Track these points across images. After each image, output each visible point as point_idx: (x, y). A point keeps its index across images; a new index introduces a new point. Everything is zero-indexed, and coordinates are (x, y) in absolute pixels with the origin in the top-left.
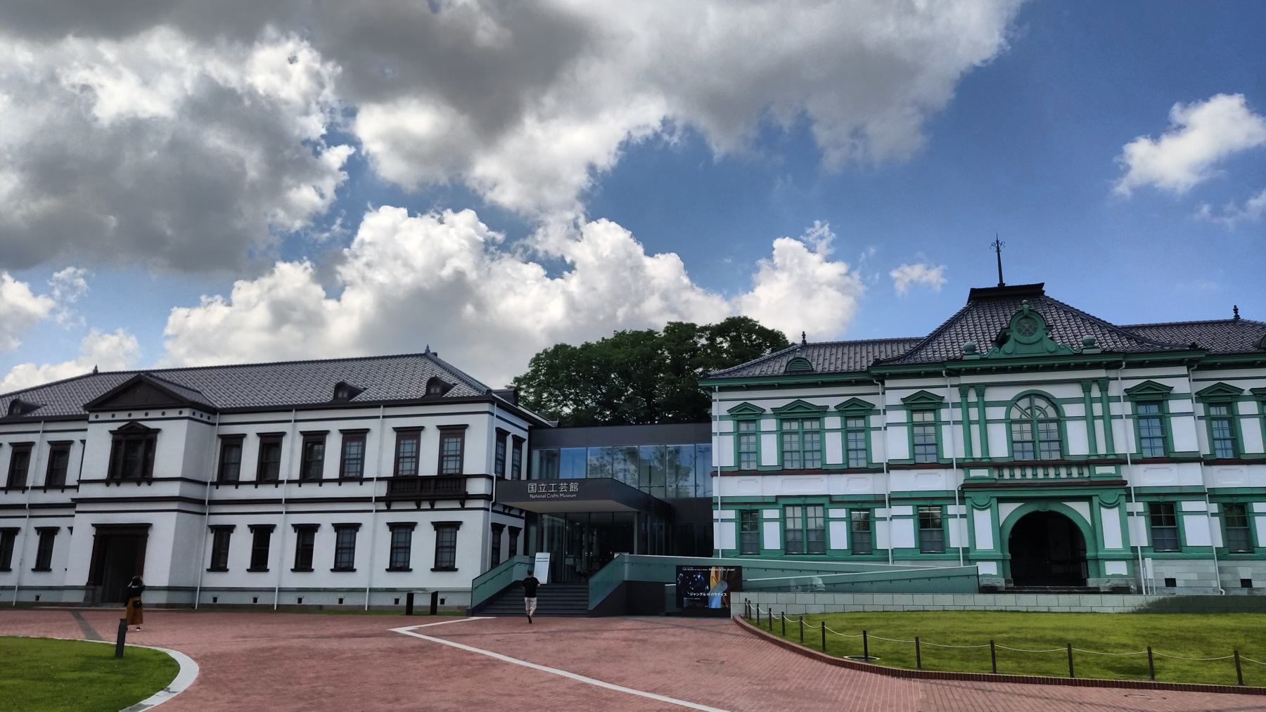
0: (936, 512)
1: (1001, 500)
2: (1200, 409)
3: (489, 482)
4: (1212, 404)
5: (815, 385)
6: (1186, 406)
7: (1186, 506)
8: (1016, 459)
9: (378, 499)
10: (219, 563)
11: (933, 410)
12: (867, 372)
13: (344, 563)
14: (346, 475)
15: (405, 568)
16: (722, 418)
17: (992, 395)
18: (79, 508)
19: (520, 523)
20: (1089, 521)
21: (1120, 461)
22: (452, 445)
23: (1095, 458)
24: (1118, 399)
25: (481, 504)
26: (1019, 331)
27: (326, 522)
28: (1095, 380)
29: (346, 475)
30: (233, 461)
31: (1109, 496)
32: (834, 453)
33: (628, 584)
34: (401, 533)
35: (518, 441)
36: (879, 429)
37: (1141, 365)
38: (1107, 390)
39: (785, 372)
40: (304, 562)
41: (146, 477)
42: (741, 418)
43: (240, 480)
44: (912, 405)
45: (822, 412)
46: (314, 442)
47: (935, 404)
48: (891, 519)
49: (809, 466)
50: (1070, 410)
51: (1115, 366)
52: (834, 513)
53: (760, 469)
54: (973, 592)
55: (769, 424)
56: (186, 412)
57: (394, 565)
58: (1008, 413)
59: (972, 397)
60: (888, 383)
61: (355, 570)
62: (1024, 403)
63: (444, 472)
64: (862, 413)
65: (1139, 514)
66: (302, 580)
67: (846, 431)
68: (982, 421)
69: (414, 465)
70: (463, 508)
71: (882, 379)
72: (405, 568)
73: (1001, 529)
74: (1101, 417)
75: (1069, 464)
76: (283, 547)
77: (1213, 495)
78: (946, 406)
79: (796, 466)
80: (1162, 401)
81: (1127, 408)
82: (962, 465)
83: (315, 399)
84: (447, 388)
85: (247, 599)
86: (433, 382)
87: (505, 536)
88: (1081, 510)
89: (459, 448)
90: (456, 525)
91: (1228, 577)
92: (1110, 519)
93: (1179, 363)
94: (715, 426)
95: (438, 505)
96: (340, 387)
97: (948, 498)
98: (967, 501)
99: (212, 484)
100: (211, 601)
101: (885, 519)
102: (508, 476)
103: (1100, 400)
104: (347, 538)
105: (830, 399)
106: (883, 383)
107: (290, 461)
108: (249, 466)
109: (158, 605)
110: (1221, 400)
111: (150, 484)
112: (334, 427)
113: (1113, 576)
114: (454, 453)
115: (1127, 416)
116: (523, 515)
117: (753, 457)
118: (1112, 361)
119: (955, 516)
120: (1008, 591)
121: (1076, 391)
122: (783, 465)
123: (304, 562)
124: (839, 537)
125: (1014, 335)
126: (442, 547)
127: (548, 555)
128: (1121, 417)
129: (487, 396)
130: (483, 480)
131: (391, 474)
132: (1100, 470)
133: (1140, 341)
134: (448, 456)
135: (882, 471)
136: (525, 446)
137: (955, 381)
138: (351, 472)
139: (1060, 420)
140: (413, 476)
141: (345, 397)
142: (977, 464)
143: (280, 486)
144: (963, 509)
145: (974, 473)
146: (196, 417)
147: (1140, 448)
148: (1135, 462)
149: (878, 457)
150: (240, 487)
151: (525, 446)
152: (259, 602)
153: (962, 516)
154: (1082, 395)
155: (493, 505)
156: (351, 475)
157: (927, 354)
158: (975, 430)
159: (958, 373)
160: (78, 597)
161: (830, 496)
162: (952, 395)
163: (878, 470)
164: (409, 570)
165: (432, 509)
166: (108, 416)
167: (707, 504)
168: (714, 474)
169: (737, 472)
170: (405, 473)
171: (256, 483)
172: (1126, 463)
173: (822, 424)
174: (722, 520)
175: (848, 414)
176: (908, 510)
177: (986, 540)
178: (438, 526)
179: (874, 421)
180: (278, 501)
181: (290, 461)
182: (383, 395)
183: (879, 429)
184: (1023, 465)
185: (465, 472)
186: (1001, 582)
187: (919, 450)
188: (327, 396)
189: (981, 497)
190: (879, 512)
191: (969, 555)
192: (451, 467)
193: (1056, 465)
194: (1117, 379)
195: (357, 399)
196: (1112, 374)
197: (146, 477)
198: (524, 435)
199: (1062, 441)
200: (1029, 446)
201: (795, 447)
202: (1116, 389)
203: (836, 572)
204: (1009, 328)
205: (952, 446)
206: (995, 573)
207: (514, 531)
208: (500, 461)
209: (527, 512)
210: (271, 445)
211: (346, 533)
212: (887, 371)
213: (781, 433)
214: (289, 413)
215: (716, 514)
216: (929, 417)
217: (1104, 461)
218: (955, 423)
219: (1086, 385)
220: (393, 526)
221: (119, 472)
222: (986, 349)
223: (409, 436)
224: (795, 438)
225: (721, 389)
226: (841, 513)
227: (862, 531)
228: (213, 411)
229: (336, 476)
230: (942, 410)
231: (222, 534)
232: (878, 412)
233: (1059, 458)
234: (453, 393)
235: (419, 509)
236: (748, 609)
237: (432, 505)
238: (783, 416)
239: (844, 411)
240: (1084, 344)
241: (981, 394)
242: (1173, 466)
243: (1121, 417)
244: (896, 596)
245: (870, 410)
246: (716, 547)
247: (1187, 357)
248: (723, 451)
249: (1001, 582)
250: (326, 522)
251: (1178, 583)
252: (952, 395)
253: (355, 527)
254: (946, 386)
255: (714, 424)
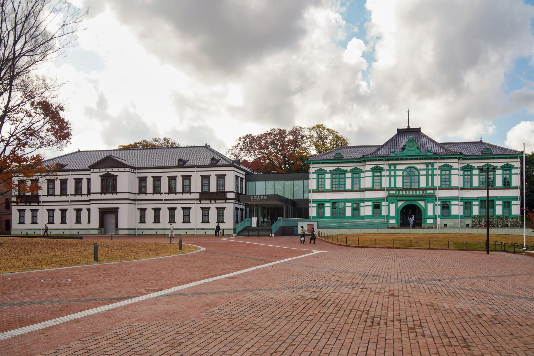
0: (448, 203)
1: (398, 201)
2: (461, 172)
3: (234, 194)
4: (504, 170)
5: (343, 163)
6: (456, 172)
7: (453, 203)
8: (404, 188)
9: (197, 199)
10: (142, 220)
11: (449, 170)
12: (360, 159)
13: (186, 220)
14: (185, 191)
15: (23, 223)
16: (313, 173)
17: (399, 167)
18: (92, 202)
19: (243, 207)
20: (424, 207)
21: (435, 189)
22: (221, 182)
23: (433, 188)
24: (436, 169)
25: (232, 201)
26: (409, 146)
27: (57, 208)
28: (430, 163)
29: (185, 191)
30: (79, 187)
31: (430, 199)
32: (349, 186)
33: (282, 227)
34: (205, 211)
35: (242, 179)
36: (363, 177)
37: (444, 158)
38: (433, 166)
39: (334, 158)
40: (172, 220)
41: (114, 191)
42: (354, 172)
43: (55, 194)
44: (374, 170)
45: (346, 171)
46: (172, 179)
47: (381, 170)
48: (365, 206)
49: (341, 189)
50: (422, 173)
51: (437, 159)
52: (348, 204)
53: (360, 190)
54: (386, 228)
55: (328, 176)
56: (127, 169)
57: (184, 221)
58: (403, 173)
59: (392, 168)
60: (367, 163)
61: (38, 223)
62: (408, 170)
63: (219, 190)
64: (358, 172)
65: (439, 205)
66: (78, 226)
67: (353, 178)
68: (433, 175)
69: (189, 188)
70: (226, 203)
71: (365, 161)
72: (23, 223)
73: (398, 210)
74: (429, 175)
75: (419, 189)
76: (164, 215)
77: (462, 199)
78: (384, 170)
79: (337, 189)
80: (510, 170)
81: (439, 172)
82: (388, 190)
83: (170, 164)
84: (218, 161)
85: (154, 232)
86: (213, 159)
87: (239, 211)
88: (422, 203)
89: (223, 182)
90: (224, 208)
91: (463, 224)
92: (430, 206)
93: (456, 158)
94: (311, 176)
95: (217, 201)
96: (180, 160)
97: (383, 200)
98: (388, 201)
99: (137, 194)
100: (141, 233)
101: (363, 206)
102: (239, 192)
103: (393, 170)
104: (221, 212)
105: (348, 167)
106: (365, 162)
107: (164, 186)
108: (150, 188)
109: (125, 234)
110: (356, 172)
111: (117, 194)
112: (179, 174)
113: (429, 223)
114: (187, 185)
115: (439, 175)
116: (244, 204)
117: (343, 186)
118: (436, 157)
119: (384, 206)
120: (398, 228)
121: (424, 167)
122: (318, 189)
123: (172, 220)
124: (349, 212)
125: (407, 148)
126: (50, 217)
127: (256, 218)
128: (436, 175)
129: (15, 172)
130: (233, 193)
131: (200, 191)
132: (429, 192)
133: (446, 150)
134: (220, 185)
135: (363, 191)
136: (244, 180)
137: (387, 162)
138: (186, 190)
139: (419, 176)
140: (36, 195)
141: (182, 164)
142: (392, 189)
143: (68, 196)
144: (387, 203)
145: (391, 192)
146: (130, 171)
147: (441, 184)
148: (439, 189)
149: (362, 187)
150: (83, 196)
151: (244, 180)
152: (65, 233)
153: (386, 206)
154: (426, 168)
155: (236, 201)
156: (51, 194)
157: (380, 153)
158: (392, 178)
159: (388, 160)
160: (96, 232)
161: (347, 199)
162: (386, 167)
163: (362, 191)
164: (24, 223)
165: (215, 203)
166: (97, 170)
167: (307, 201)
168: (310, 192)
169: (317, 191)
170: (220, 190)
171: (60, 195)
172: (436, 189)
173: (325, 176)
174: (312, 207)
175: (374, 171)
176: (370, 204)
177: (393, 213)
178: (218, 208)
179: (362, 175)
180: (68, 201)
181: (164, 186)
182: (195, 163)
183: (363, 177)
184: (406, 190)
185: (226, 191)
186: (396, 226)
187: (444, 183)
188: (209, 163)
189: (392, 199)
190: (362, 204)
191: (388, 217)
192: (221, 189)
193: (416, 190)
194: (437, 163)
195: (64, 169)
196: (435, 161)
197: (114, 191)
198: (244, 177)
199: (471, 182)
200: (409, 184)
201: (337, 183)
202: (436, 166)
203: (346, 223)
204: (405, 145)
205: (385, 184)
206: (395, 223)
207: (242, 210)
208: (237, 186)
209: (245, 204)
210: (157, 180)
211: (186, 211)
212: (366, 159)
213: (332, 178)
214: (163, 169)
215: (310, 205)
216: (379, 174)
217: (430, 189)
218: (386, 176)
219: (427, 165)
220: (202, 208)
221: (105, 190)
222: (398, 152)
223: (205, 178)
224: (336, 180)
225: (313, 163)
226: (350, 204)
227: (356, 209)
228: (135, 168)
229: (181, 191)
230: (383, 172)
231: (143, 211)
232: (363, 172)
233: (417, 187)
234: (220, 163)
235: (211, 203)
236: (319, 234)
237: (215, 202)
238: (333, 173)
239: (352, 171)
240: (428, 151)
241: (395, 167)
242: (450, 191)
243: (436, 175)
244: (362, 230)
245: (361, 171)
246: (310, 215)
247: (458, 156)
248: (313, 184)
249: (396, 226)
250: (179, 207)
251: (448, 226)
252: (386, 167)
253: (189, 209)
254: (385, 164)
255: (310, 175)
